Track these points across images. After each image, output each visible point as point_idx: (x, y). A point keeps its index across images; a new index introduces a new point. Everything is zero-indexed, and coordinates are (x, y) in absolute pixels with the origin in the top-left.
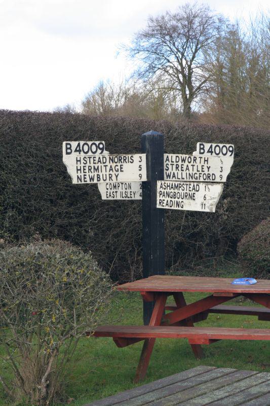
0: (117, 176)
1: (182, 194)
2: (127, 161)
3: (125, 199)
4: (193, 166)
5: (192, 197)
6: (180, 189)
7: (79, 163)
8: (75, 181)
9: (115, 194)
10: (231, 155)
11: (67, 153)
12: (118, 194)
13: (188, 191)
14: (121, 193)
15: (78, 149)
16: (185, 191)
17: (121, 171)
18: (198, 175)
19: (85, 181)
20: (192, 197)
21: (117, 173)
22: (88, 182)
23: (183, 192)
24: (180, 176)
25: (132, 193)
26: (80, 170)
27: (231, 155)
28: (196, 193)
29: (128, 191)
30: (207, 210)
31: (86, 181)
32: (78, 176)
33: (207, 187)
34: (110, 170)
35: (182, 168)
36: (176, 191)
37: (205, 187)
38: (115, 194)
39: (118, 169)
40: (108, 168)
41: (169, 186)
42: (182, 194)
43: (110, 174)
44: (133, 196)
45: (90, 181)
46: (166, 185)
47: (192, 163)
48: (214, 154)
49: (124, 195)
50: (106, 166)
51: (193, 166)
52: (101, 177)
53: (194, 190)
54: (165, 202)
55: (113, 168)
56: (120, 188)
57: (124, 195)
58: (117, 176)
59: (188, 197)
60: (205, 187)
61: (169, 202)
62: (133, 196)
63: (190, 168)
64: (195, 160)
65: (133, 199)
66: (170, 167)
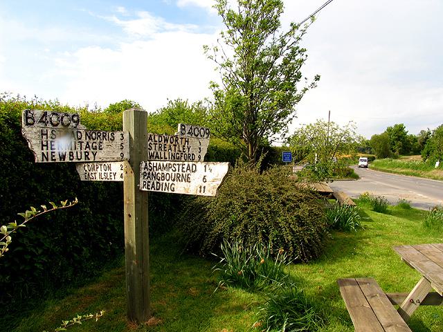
0: (95, 155)
1: (173, 175)
2: (107, 138)
3: (104, 180)
4: (175, 145)
5: (188, 180)
6: (171, 169)
7: (45, 148)
8: (83, 179)
9: (93, 175)
10: (207, 138)
11: (27, 124)
12: (97, 176)
13: (181, 173)
14: (100, 174)
15: (44, 119)
16: (177, 172)
17: (100, 149)
18: (179, 155)
19: (52, 160)
20: (188, 180)
21: (95, 151)
22: (58, 161)
23: (174, 173)
24: (162, 156)
25: (112, 175)
26: (47, 146)
27: (207, 138)
28: (192, 174)
29: (108, 172)
30: (207, 194)
31: (55, 160)
32: (43, 153)
33: (207, 166)
34: (86, 147)
35: (165, 147)
36: (165, 172)
37: (205, 166)
38: (93, 175)
39: (96, 146)
40: (84, 145)
41: (156, 167)
42: (173, 175)
43: (85, 152)
44: (113, 177)
45: (61, 160)
46: (152, 166)
47: (174, 143)
48: (193, 135)
49: (103, 176)
50: (81, 143)
51: (175, 145)
52: (75, 155)
53: (188, 171)
54: (151, 184)
55: (90, 145)
56: (99, 169)
57: (103, 176)
58: (95, 155)
59: (180, 179)
60: (205, 166)
61: (155, 184)
62: (113, 177)
63: (173, 148)
64: (176, 141)
65: (113, 180)
66: (153, 146)
